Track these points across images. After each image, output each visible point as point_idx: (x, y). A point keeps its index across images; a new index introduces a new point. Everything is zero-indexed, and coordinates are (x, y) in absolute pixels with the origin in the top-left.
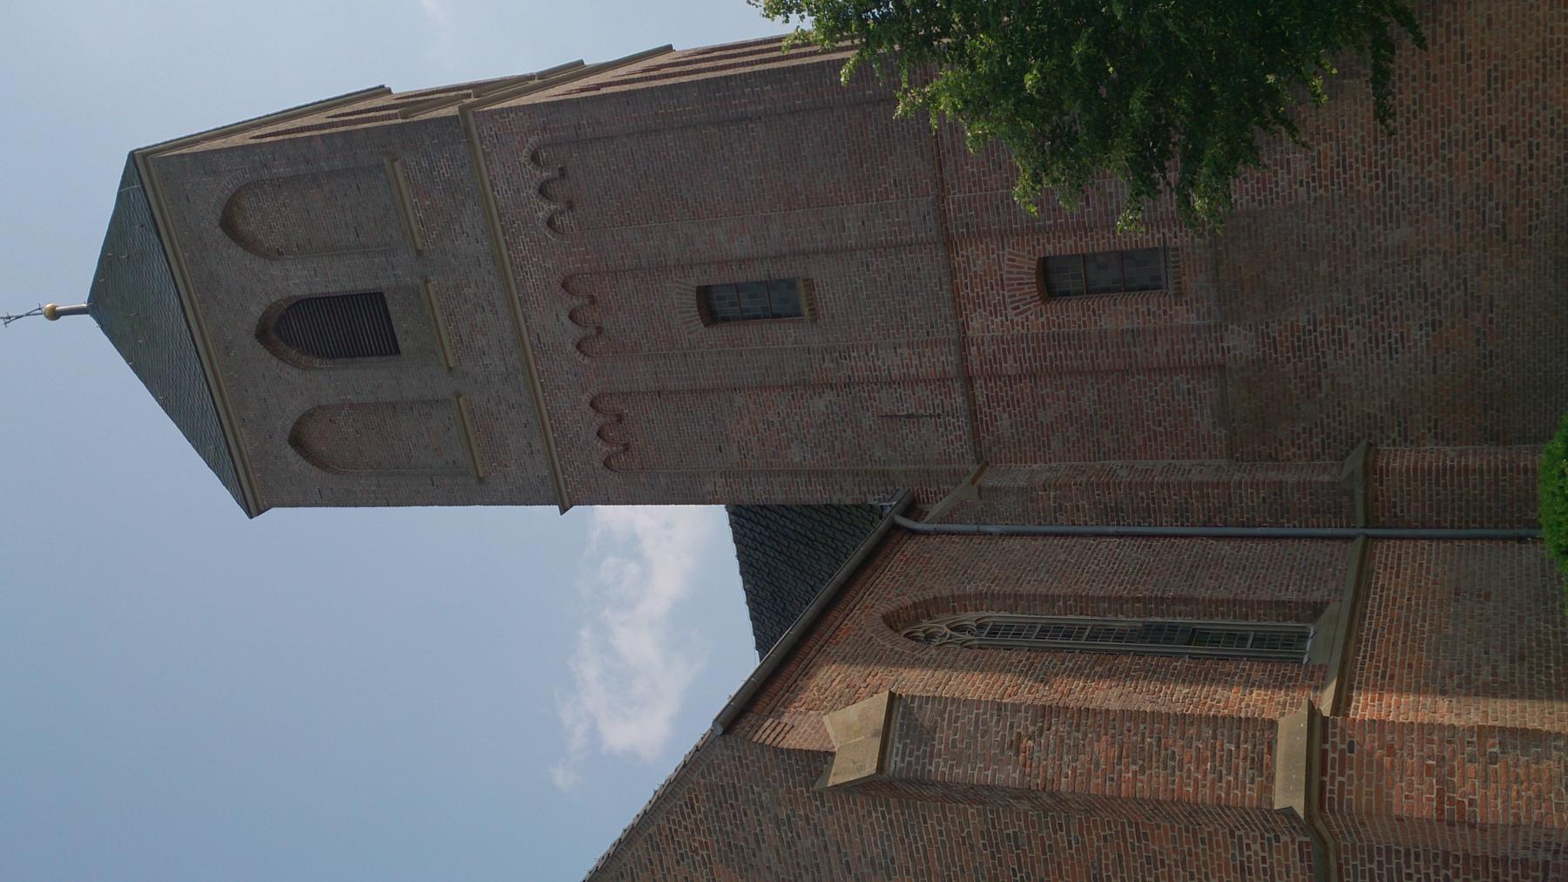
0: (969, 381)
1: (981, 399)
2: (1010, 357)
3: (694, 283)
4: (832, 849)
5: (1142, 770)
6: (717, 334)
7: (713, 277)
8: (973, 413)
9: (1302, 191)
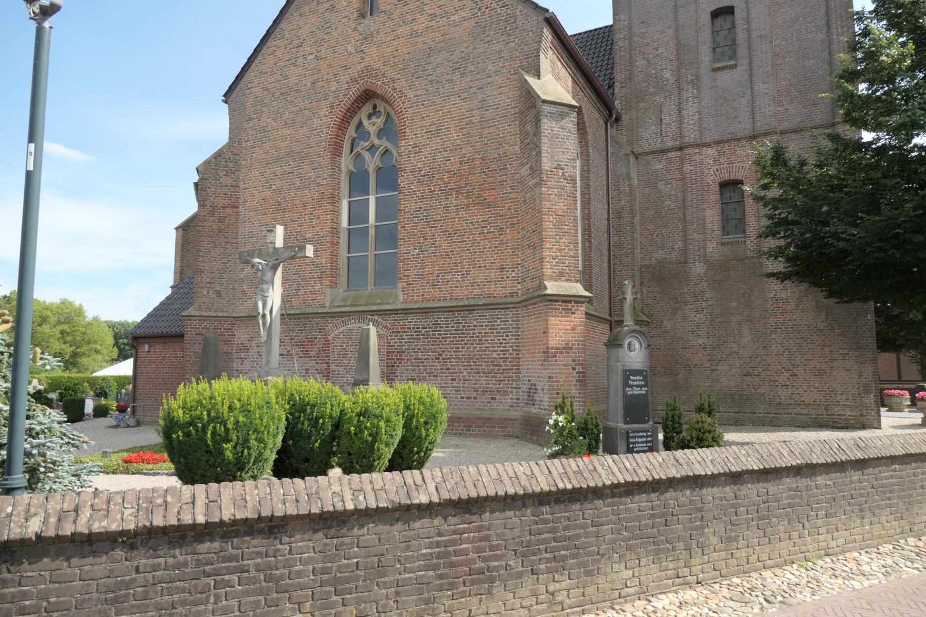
0: (680, 149)
1: (670, 155)
2: (692, 168)
3: (736, 4)
4: (489, 80)
5: (554, 225)
6: (706, 17)
7: (739, 15)
8: (663, 151)
9: (772, 295)
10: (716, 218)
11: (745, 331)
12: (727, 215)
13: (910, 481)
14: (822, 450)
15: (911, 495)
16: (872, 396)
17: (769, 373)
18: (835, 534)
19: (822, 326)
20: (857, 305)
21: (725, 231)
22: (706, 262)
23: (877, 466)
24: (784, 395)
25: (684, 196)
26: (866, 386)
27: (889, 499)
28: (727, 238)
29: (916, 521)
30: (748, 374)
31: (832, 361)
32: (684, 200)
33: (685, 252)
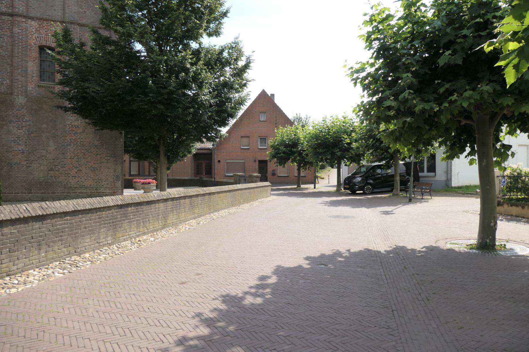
0: (12, 15)
2: (20, 31)
10: (35, 69)
11: (51, 143)
12: (44, 69)
13: (77, 225)
14: (11, 211)
15: (77, 233)
16: (120, 182)
17: (65, 169)
18: (16, 262)
19: (97, 143)
20: (116, 133)
21: (42, 77)
22: (26, 96)
23: (54, 218)
24: (73, 182)
25: (12, 49)
26: (117, 176)
27: (61, 236)
28: (42, 83)
29: (79, 246)
30: (51, 170)
31: (101, 163)
32: (12, 51)
33: (11, 87)
